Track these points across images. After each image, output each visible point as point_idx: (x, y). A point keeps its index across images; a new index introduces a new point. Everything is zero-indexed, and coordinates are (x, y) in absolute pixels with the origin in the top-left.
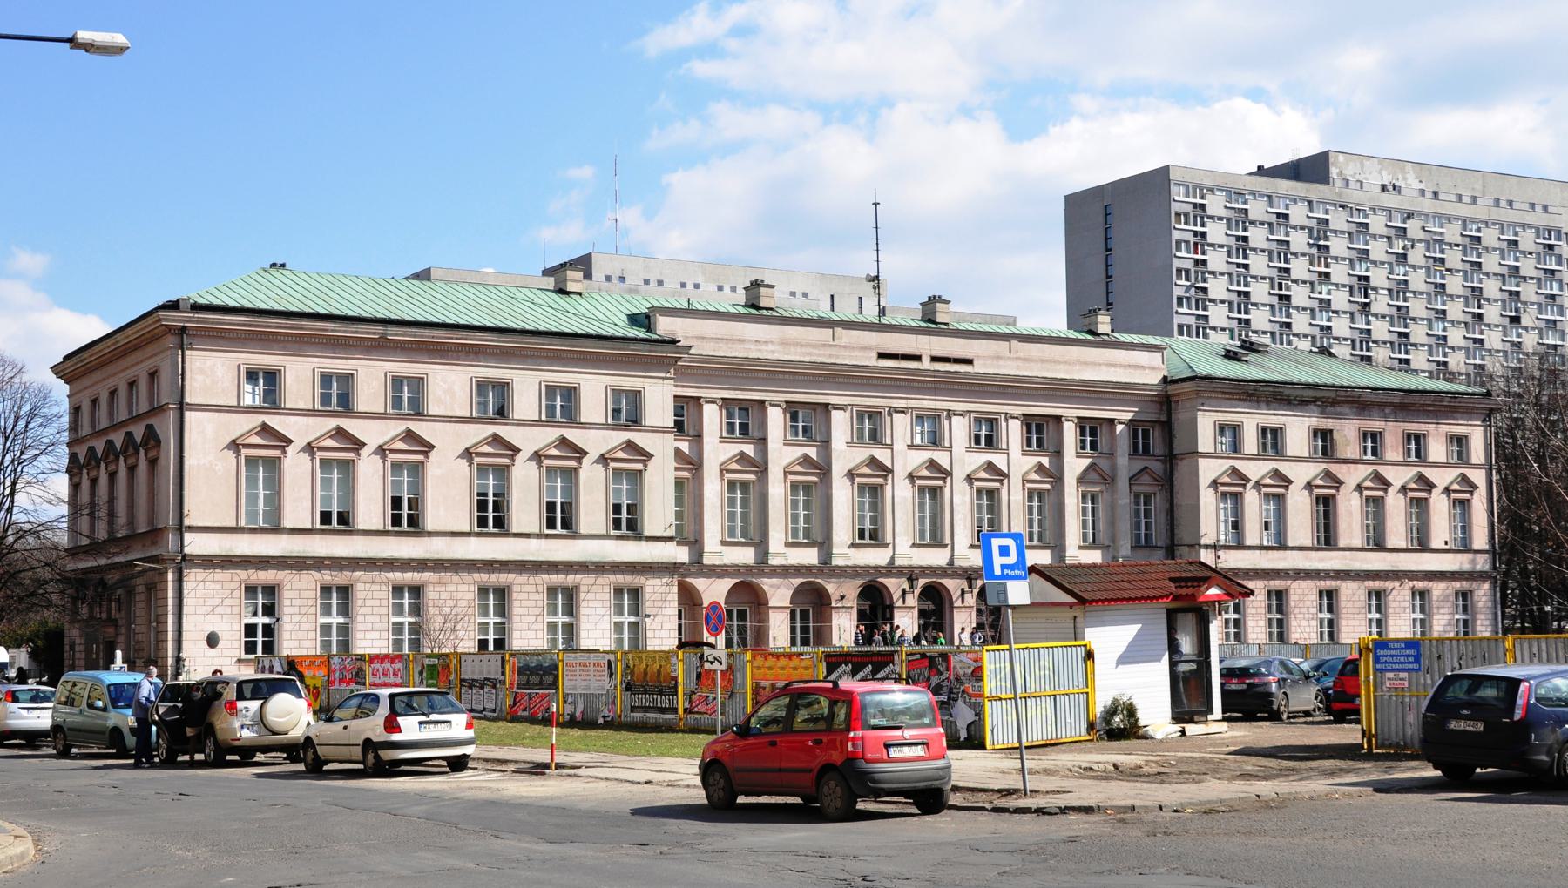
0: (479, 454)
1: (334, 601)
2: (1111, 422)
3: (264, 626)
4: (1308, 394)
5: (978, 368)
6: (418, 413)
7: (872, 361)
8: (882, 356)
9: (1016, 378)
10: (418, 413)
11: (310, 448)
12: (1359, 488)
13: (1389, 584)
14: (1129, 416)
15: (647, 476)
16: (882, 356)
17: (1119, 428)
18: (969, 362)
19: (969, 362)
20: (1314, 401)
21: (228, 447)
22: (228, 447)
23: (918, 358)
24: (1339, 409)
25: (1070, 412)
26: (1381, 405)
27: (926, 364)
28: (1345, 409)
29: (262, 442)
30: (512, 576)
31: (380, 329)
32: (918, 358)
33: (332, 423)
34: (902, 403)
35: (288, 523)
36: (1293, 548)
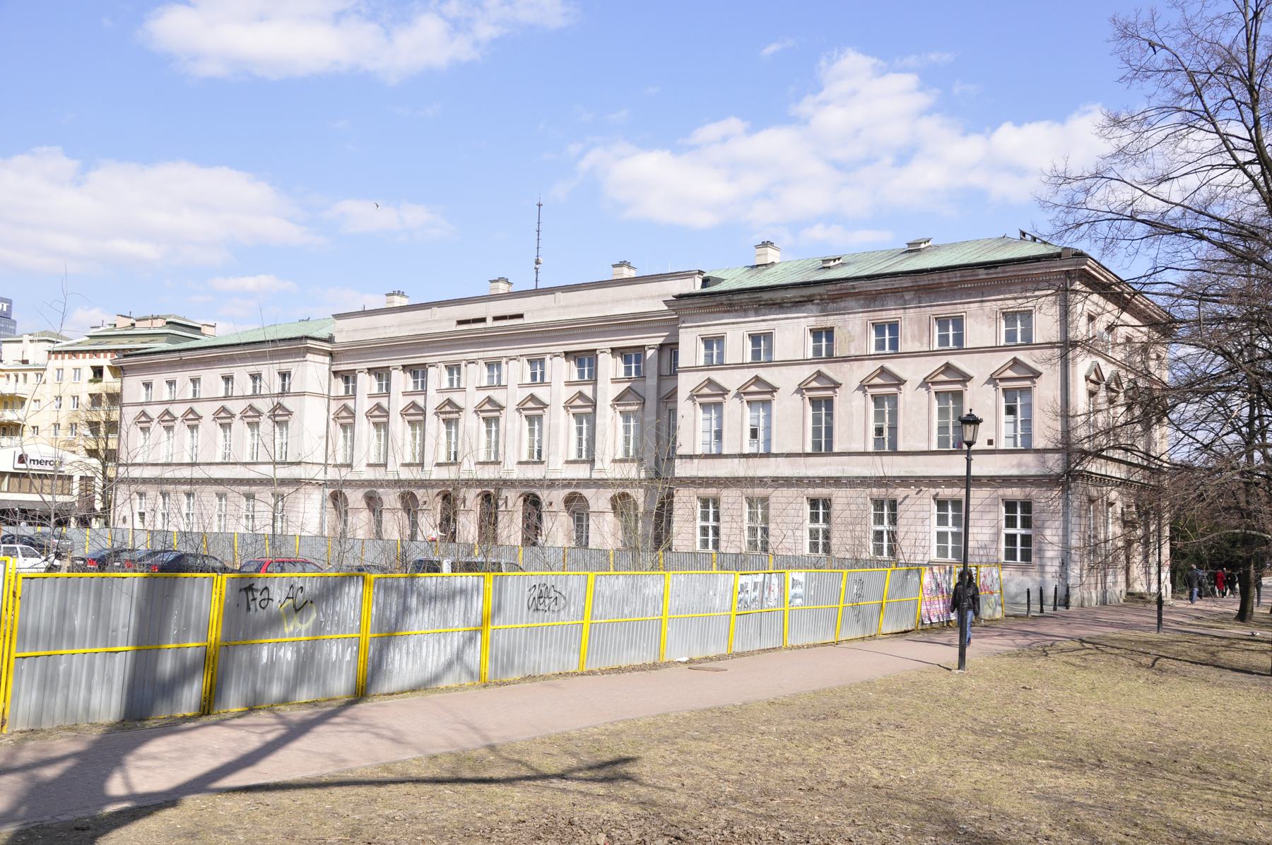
0: (1002, 380)
1: (950, 513)
2: (642, 348)
3: (1022, 536)
4: (881, 285)
5: (527, 320)
6: (960, 347)
7: (453, 327)
8: (460, 322)
9: (559, 323)
10: (960, 347)
11: (993, 380)
12: (863, 387)
13: (899, 493)
14: (660, 341)
15: (901, 397)
16: (460, 322)
17: (650, 353)
18: (521, 316)
19: (521, 316)
20: (810, 300)
21: (988, 382)
22: (988, 382)
23: (483, 320)
24: (843, 304)
25: (602, 344)
26: (895, 292)
27: (490, 323)
28: (851, 303)
29: (1015, 375)
30: (770, 490)
31: (177, 354)
32: (483, 320)
33: (942, 361)
34: (474, 356)
35: (901, 448)
36: (776, 455)
